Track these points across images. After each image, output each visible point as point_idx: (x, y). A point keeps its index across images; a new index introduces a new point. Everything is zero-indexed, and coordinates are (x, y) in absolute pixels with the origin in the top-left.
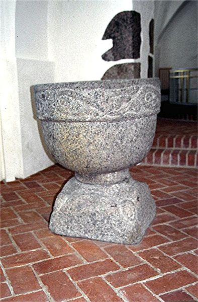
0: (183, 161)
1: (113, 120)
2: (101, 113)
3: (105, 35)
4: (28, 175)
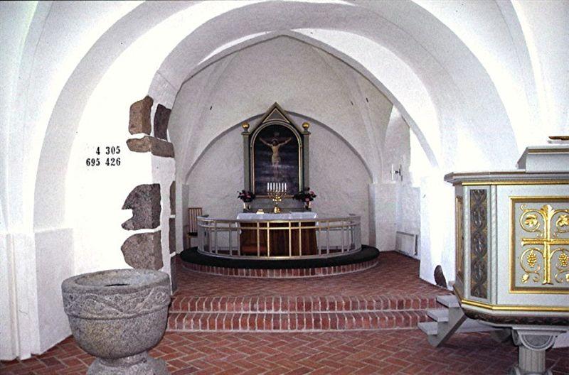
0: (204, 326)
1: (130, 318)
2: (120, 313)
3: (124, 205)
4: (45, 350)
